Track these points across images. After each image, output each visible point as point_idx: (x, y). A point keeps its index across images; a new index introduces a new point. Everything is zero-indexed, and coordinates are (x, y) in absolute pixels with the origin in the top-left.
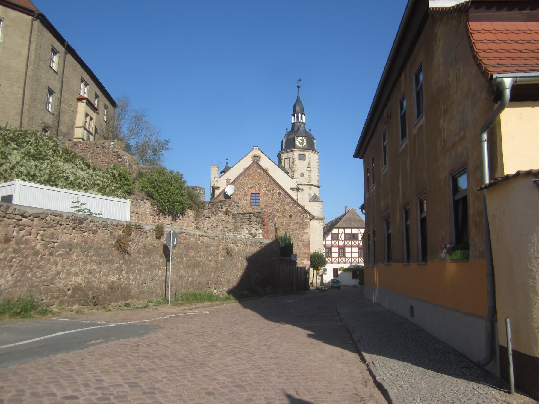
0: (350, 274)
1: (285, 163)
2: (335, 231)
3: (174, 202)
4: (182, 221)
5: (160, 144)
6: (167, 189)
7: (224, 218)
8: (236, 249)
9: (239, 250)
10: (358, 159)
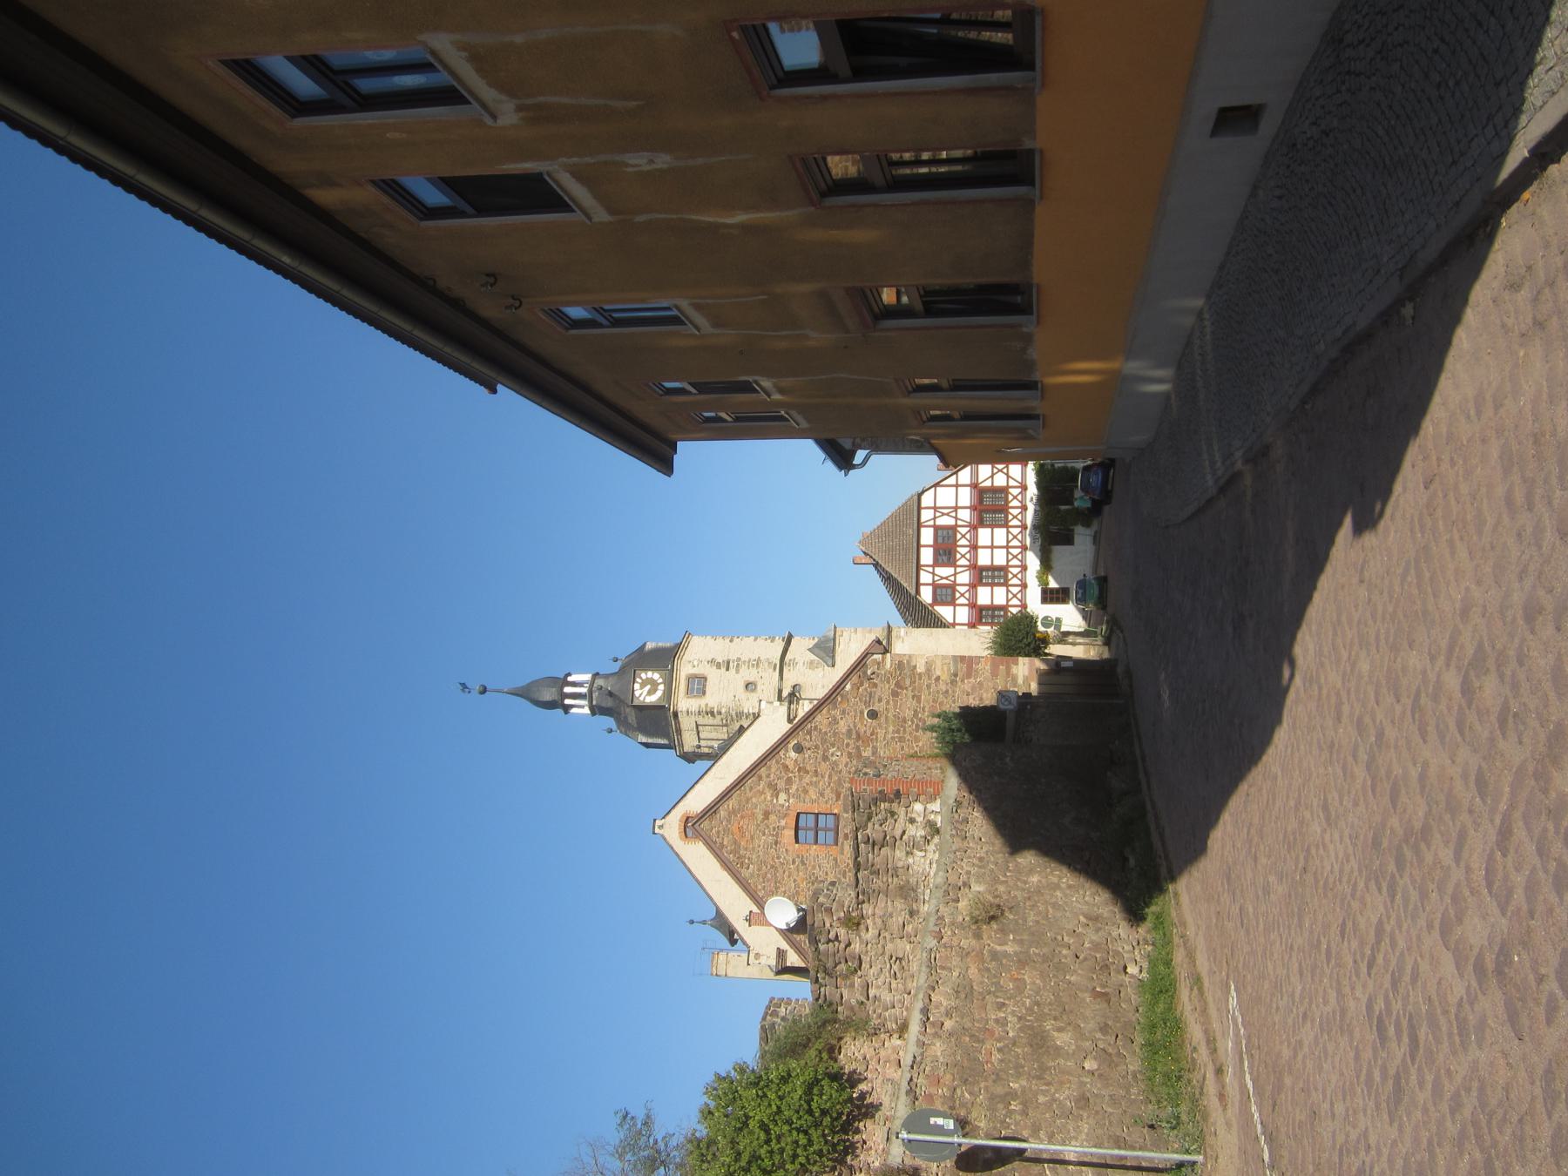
0: (1059, 551)
1: (713, 736)
2: (926, 595)
3: (810, 1112)
4: (877, 1083)
5: (628, 1146)
6: (763, 1136)
7: (872, 932)
8: (976, 888)
9: (980, 878)
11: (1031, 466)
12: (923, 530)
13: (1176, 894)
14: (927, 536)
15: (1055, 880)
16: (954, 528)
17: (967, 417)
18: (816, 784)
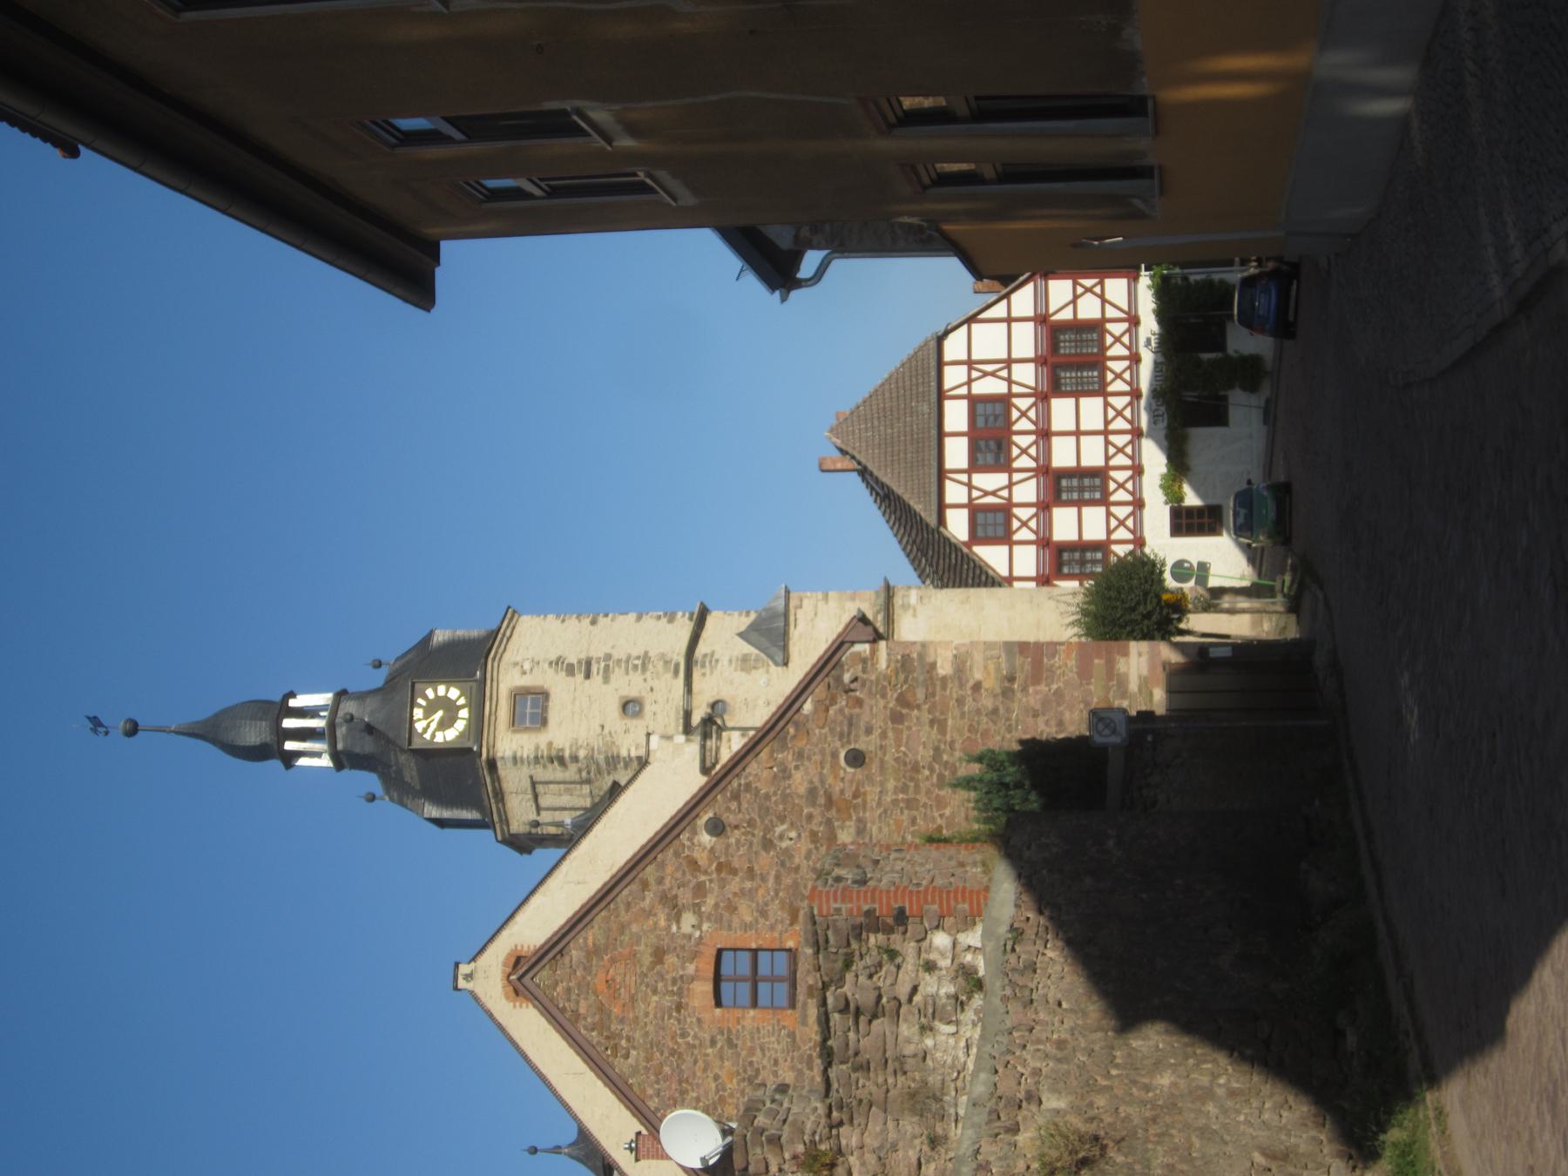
0: (1202, 439)
1: (562, 806)
2: (957, 526)
8: (1052, 1102)
10: (443, 277)
11: (1145, 280)
12: (949, 405)
13: (1440, 1113)
14: (956, 416)
15: (1205, 1080)
16: (1005, 401)
17: (1010, 174)
18: (750, 894)
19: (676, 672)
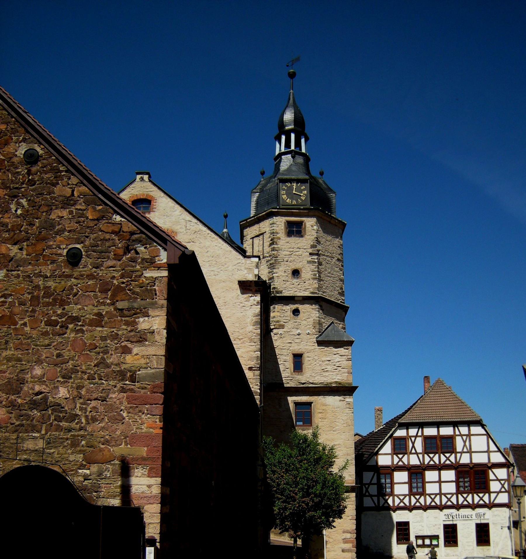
2: (401, 433)
19: (312, 293)
